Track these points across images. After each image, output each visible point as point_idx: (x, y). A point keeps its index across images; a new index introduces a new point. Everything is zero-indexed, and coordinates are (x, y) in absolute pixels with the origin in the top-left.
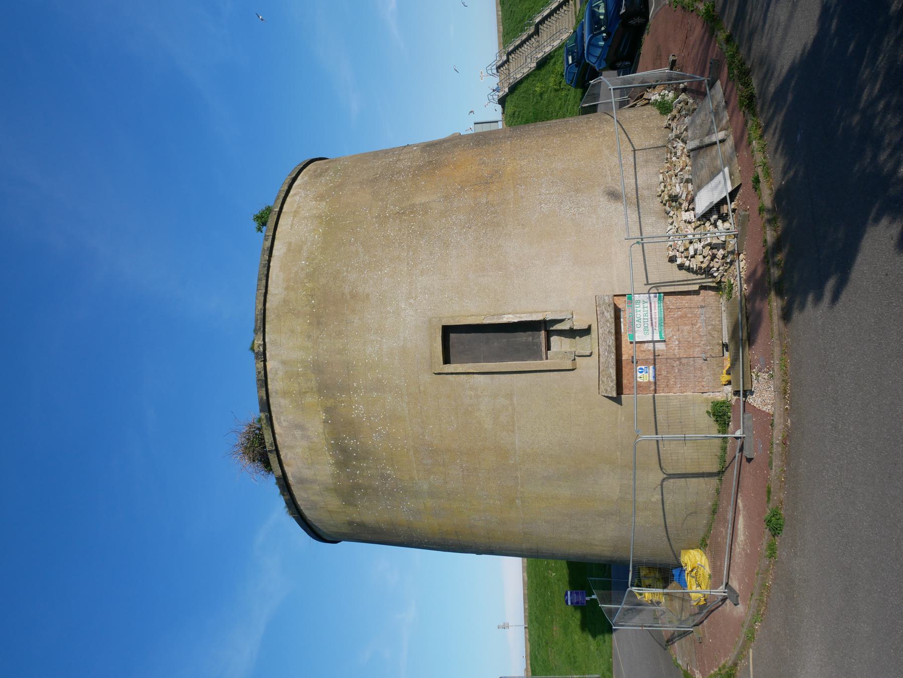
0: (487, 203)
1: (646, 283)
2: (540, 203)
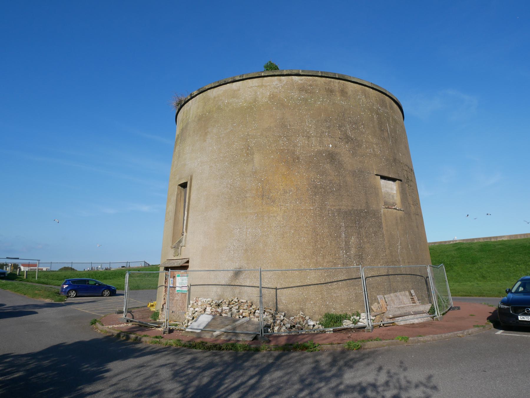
0: (246, 197)
1: (191, 285)
2: (240, 228)
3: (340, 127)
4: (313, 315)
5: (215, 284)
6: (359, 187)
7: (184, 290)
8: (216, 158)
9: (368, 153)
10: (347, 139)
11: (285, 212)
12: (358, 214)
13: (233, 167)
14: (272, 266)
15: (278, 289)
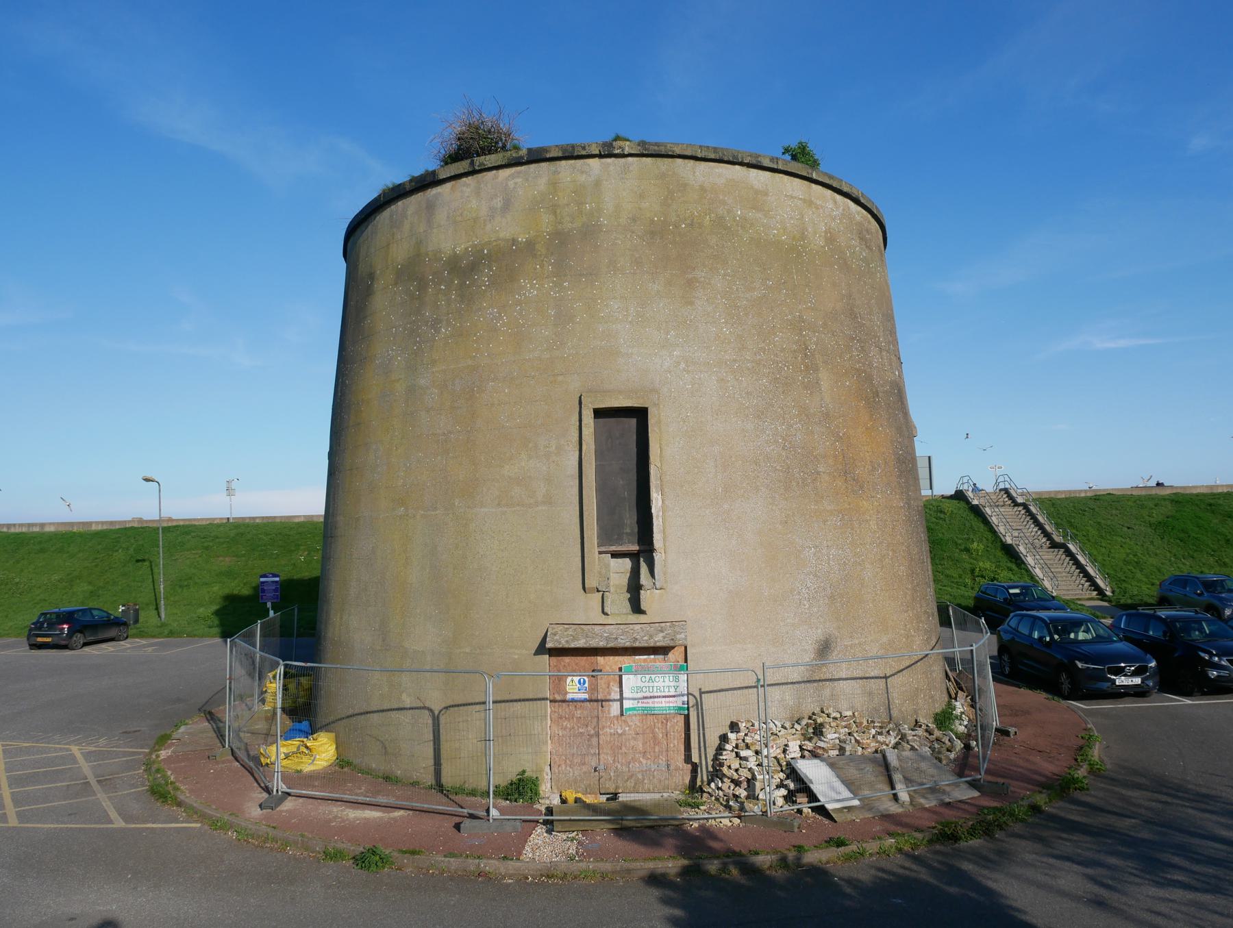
0: (818, 473)
1: (703, 690)
7: (660, 705)
8: (735, 361)
13: (783, 393)
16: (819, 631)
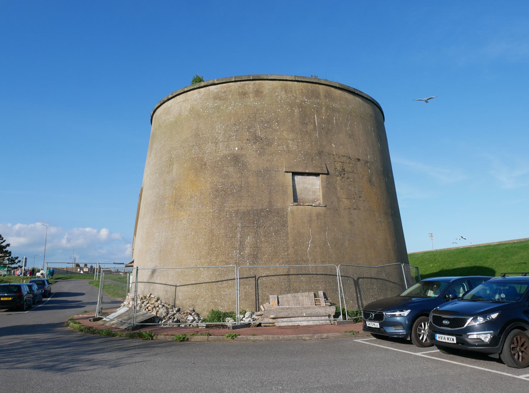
3: (249, 128)
4: (202, 311)
5: (141, 281)
6: (263, 186)
9: (280, 151)
10: (256, 139)
11: (189, 216)
12: (257, 214)
14: (175, 265)
15: (177, 286)
16: (154, 264)
